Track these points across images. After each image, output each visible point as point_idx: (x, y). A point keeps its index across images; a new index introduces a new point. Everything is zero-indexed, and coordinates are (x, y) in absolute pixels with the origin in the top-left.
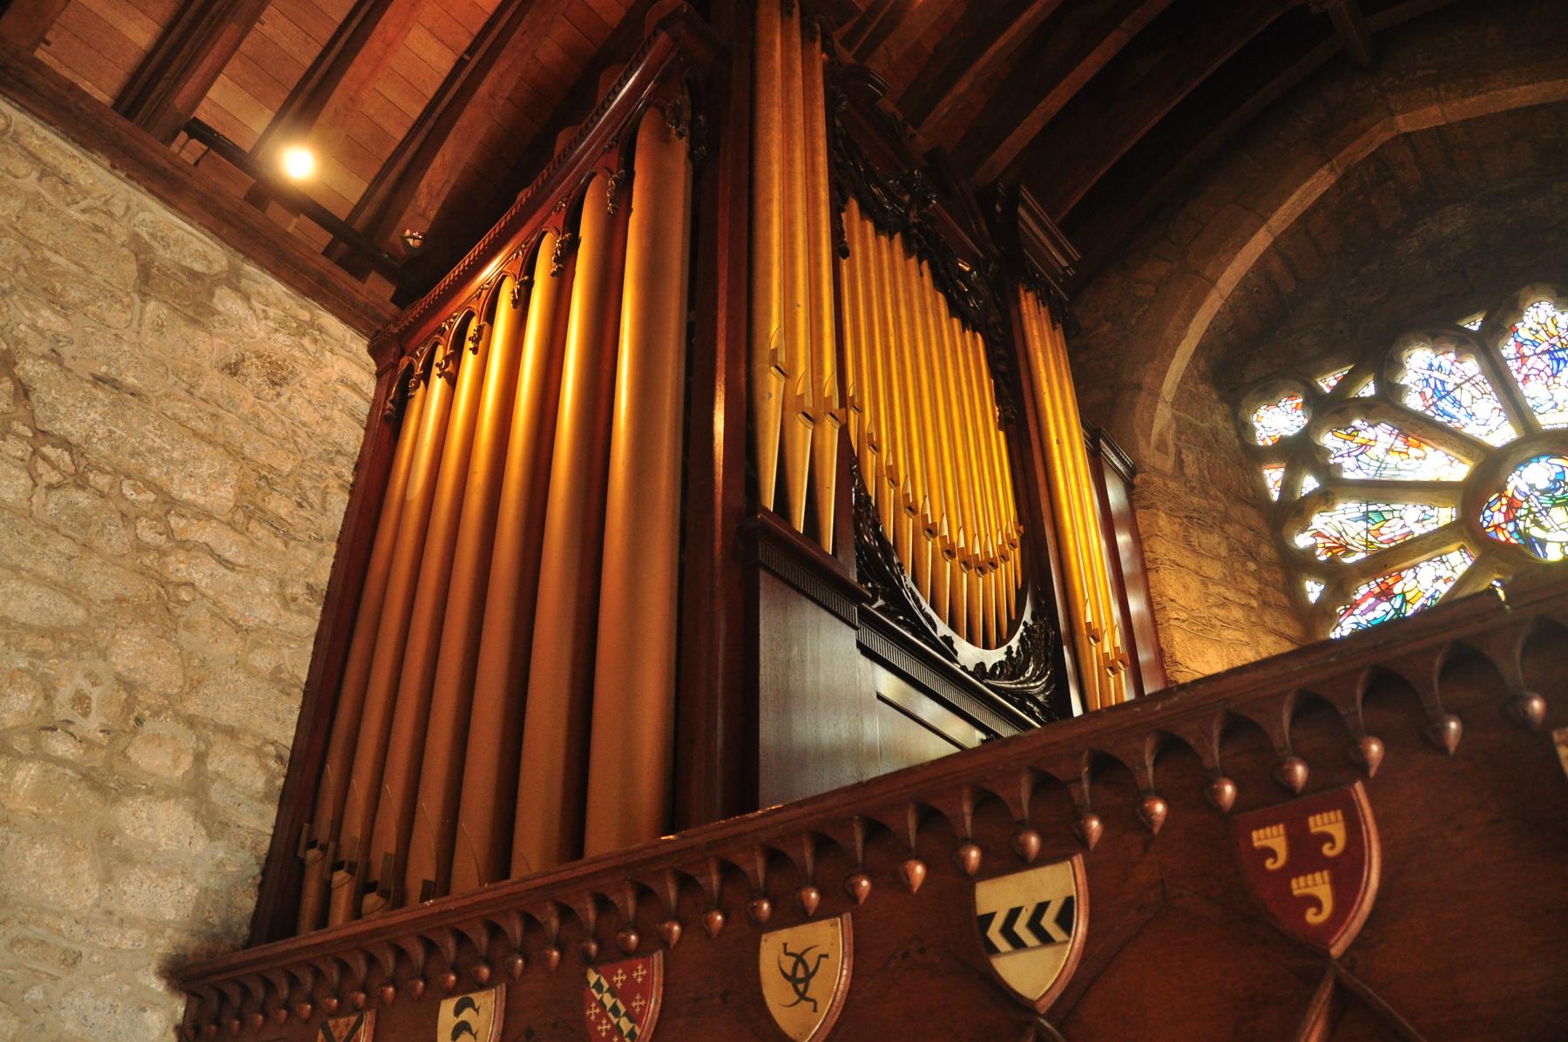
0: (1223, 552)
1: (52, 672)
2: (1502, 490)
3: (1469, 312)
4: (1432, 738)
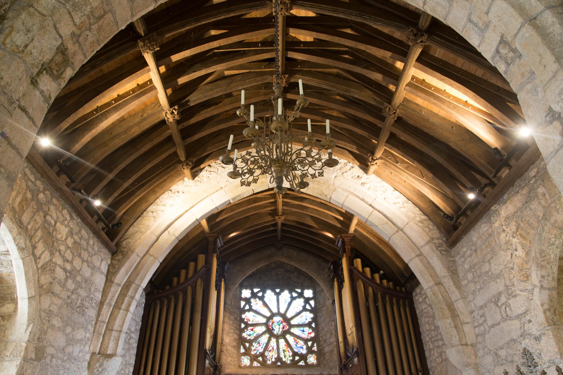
1: (302, 104)
2: (272, 319)
3: (277, 288)
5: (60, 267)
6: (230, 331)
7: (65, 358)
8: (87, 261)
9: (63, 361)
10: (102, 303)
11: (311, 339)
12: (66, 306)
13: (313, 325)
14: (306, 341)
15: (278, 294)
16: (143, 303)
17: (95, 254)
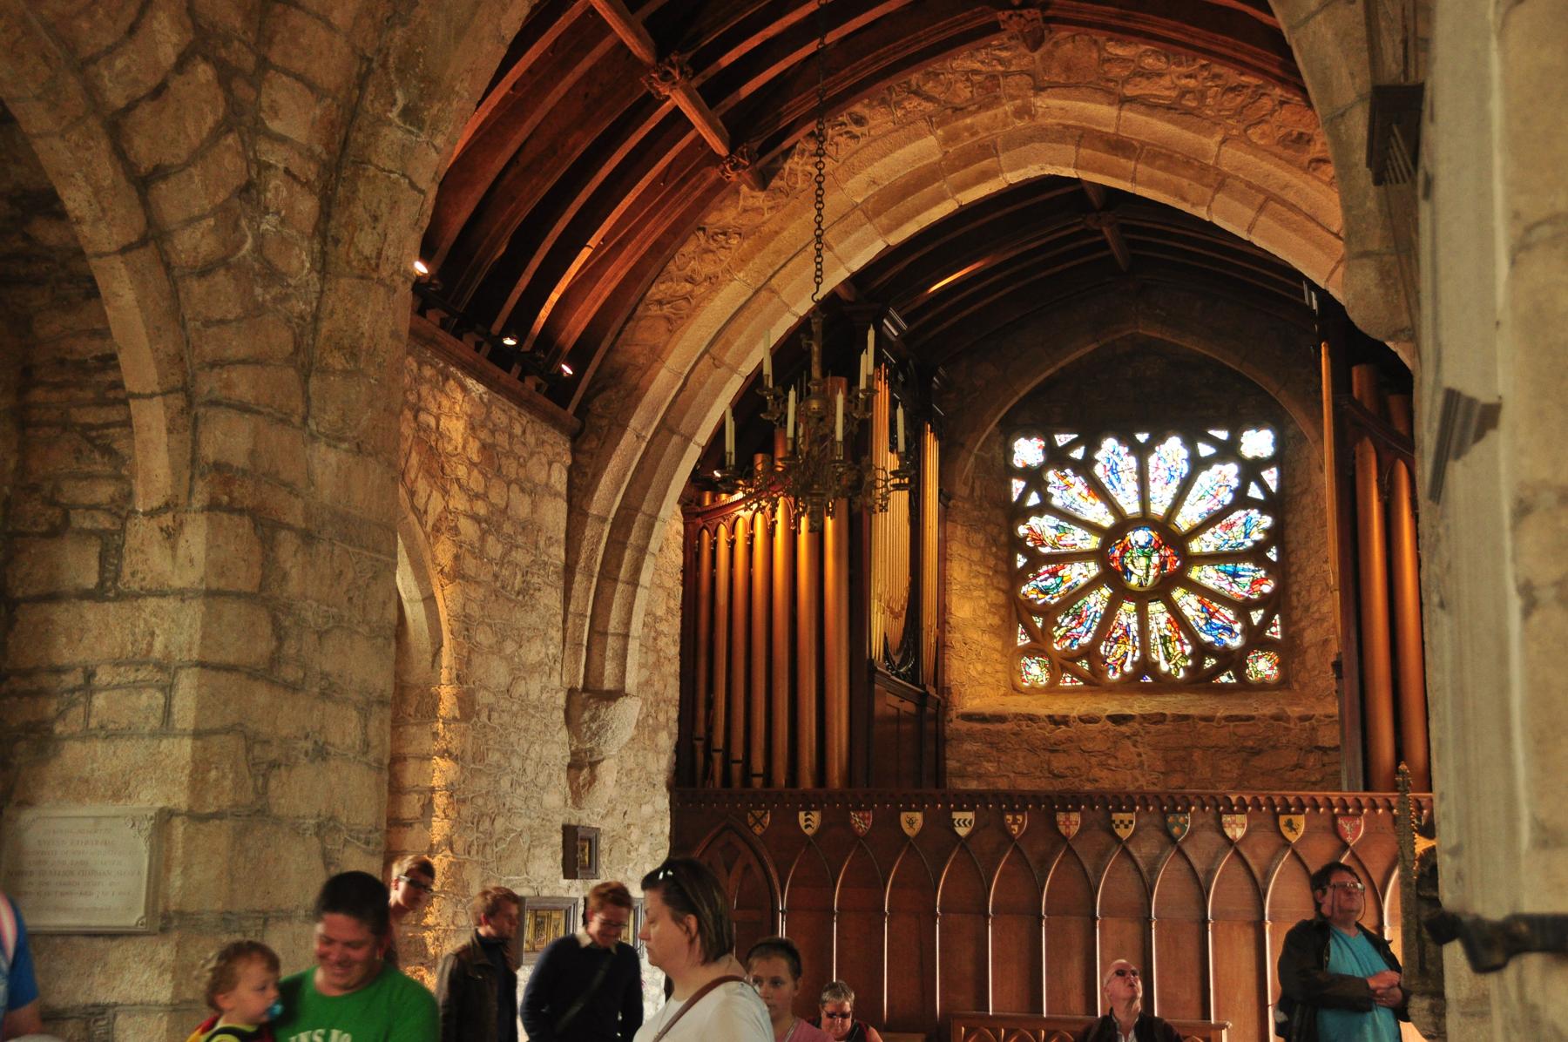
0: (982, 544)
3: (1142, 431)
4: (1040, 807)
5: (467, 516)
6: (974, 581)
7: (515, 708)
8: (517, 481)
9: (515, 715)
10: (569, 571)
11: (1265, 602)
12: (493, 598)
13: (1272, 555)
14: (1243, 608)
15: (1142, 453)
16: (678, 533)
17: (532, 454)
